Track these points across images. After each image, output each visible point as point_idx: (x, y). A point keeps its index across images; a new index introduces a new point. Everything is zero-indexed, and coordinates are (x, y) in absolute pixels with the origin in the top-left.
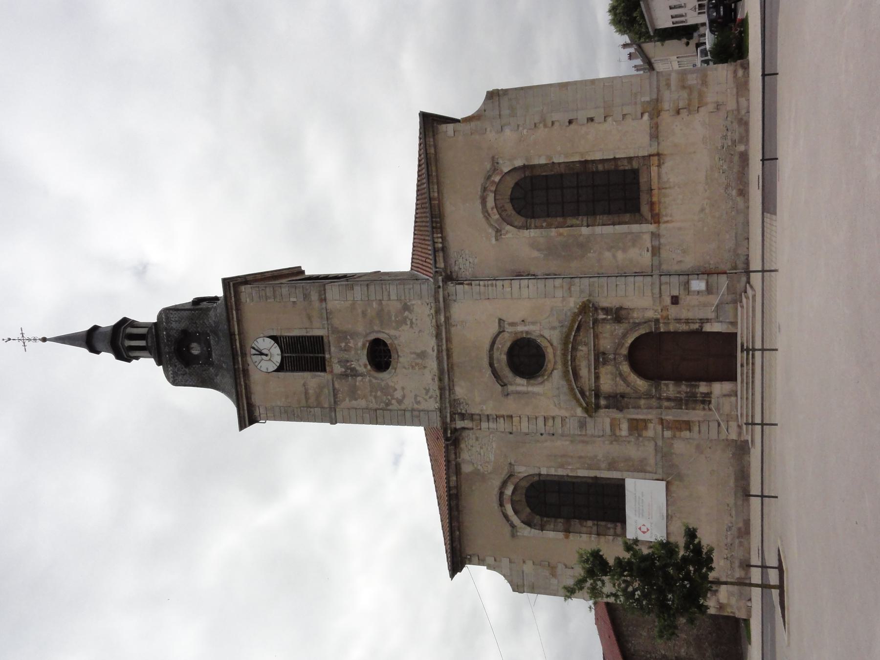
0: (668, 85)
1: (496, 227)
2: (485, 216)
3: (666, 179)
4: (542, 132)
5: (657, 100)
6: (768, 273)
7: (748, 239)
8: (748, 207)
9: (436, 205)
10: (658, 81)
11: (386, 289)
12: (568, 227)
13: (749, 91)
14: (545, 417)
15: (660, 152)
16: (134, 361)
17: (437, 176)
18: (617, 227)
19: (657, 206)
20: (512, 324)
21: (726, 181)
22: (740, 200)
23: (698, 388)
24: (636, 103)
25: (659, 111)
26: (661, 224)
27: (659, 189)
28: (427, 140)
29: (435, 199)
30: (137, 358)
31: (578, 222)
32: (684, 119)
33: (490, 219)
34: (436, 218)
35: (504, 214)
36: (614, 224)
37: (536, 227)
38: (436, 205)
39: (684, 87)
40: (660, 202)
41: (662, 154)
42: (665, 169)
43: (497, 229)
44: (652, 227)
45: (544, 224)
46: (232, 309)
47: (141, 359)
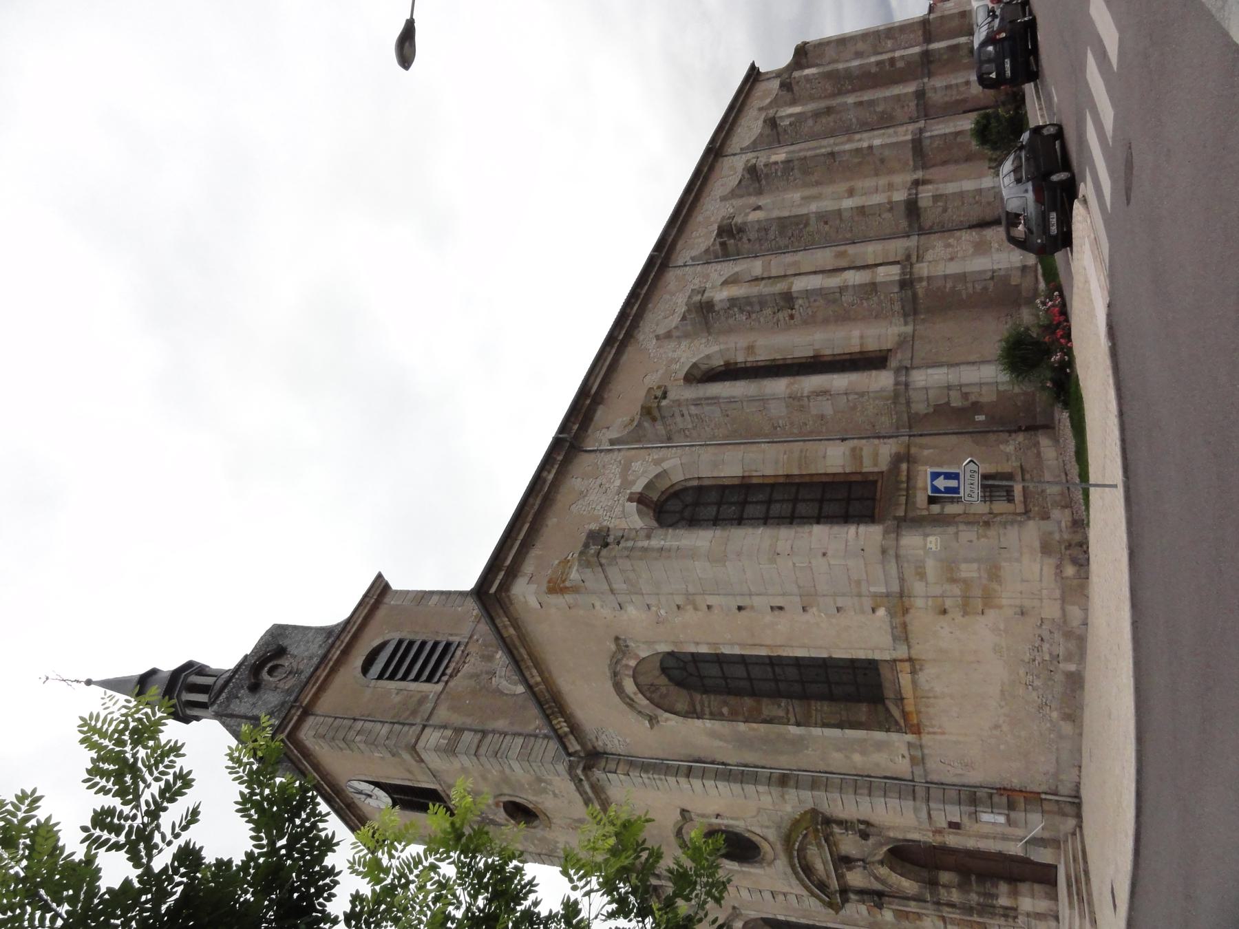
0: (922, 575)
1: (648, 715)
2: (627, 704)
3: (927, 688)
4: (690, 616)
5: (901, 595)
6: (1098, 489)
7: (1080, 767)
8: (1081, 735)
9: (544, 691)
10: (900, 568)
11: (505, 763)
12: (765, 721)
13: (1088, 597)
14: (772, 892)
15: (914, 657)
16: (194, 722)
17: (530, 654)
18: (847, 731)
19: (915, 715)
20: (703, 816)
21: (1040, 700)
22: (1067, 728)
23: (997, 899)
24: (859, 595)
25: (907, 609)
26: (922, 735)
27: (915, 697)
28: (497, 621)
29: (538, 684)
30: (198, 719)
31: (781, 713)
32: (956, 621)
33: (635, 705)
34: (547, 703)
35: (655, 696)
36: (840, 726)
37: (714, 716)
38: (544, 691)
39: (953, 580)
40: (918, 712)
41: (916, 660)
42: (922, 677)
43: (651, 716)
44: (910, 737)
45: (725, 710)
46: (300, 760)
47: (204, 720)
